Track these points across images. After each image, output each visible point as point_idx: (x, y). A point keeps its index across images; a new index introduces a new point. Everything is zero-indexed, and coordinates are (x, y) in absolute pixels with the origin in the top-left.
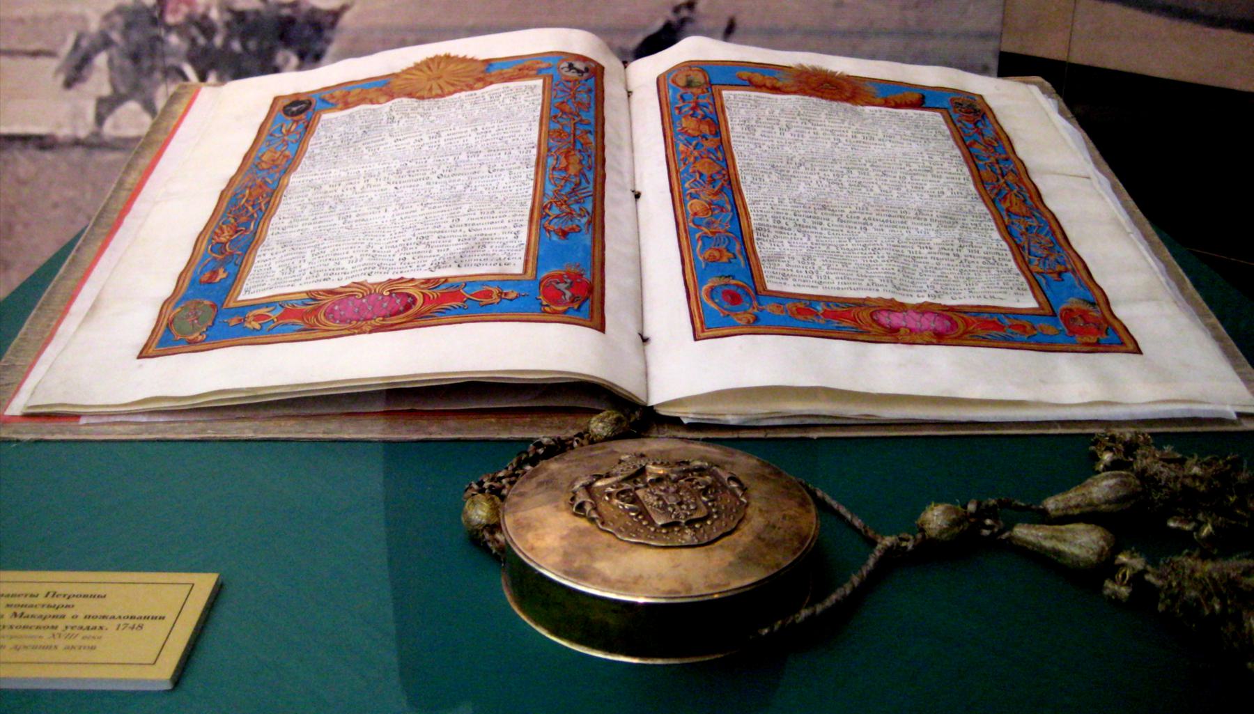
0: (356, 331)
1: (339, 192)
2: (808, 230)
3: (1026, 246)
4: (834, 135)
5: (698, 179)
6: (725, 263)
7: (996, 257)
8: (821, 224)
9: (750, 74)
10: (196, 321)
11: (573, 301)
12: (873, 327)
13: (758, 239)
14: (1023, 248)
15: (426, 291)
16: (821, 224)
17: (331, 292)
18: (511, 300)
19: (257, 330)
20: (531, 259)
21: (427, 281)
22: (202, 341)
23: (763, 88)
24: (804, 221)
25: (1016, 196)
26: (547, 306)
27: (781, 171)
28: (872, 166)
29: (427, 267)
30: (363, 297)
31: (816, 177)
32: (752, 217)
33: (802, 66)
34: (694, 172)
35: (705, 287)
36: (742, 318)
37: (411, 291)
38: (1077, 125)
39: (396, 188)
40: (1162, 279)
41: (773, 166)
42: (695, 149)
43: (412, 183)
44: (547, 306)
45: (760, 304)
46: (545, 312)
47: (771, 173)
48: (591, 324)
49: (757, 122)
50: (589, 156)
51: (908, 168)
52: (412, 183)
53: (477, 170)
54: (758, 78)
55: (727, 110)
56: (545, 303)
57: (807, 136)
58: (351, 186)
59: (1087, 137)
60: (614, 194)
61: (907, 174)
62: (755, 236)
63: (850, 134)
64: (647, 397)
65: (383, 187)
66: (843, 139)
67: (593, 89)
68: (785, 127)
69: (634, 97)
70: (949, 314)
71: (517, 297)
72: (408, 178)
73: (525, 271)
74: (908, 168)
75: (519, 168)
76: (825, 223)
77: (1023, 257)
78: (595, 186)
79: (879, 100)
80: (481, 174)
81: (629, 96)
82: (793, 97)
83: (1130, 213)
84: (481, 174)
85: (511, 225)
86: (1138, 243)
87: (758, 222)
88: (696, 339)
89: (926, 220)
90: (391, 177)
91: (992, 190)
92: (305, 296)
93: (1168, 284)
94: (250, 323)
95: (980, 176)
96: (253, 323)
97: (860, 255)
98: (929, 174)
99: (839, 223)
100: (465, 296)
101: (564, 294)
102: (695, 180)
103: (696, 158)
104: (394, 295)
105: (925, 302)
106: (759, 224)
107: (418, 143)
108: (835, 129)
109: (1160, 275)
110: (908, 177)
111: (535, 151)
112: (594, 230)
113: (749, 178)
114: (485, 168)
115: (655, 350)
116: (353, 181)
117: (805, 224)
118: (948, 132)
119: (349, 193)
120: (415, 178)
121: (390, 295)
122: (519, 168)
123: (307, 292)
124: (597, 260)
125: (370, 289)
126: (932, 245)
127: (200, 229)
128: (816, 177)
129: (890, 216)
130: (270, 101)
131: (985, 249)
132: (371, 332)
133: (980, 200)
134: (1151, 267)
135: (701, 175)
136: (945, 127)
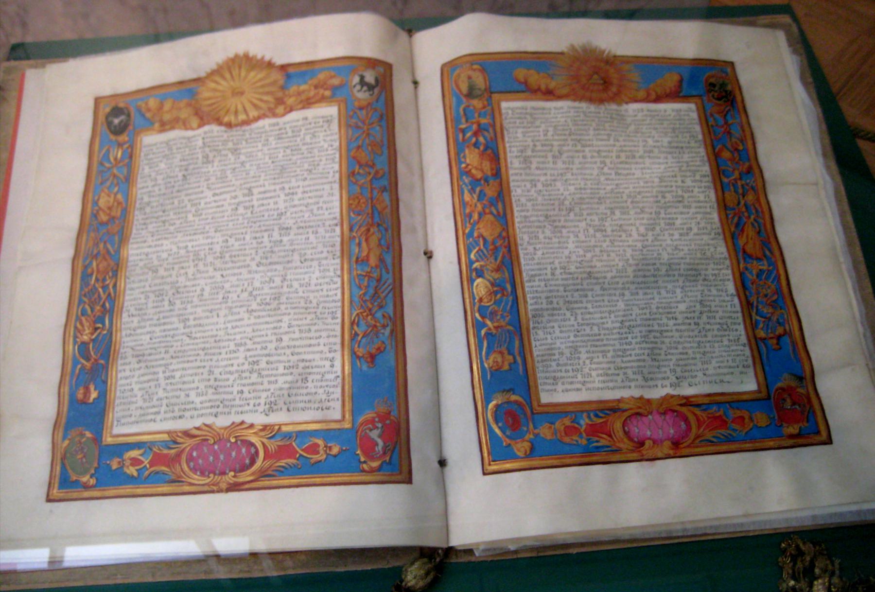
0: (215, 488)
1: (174, 278)
2: (576, 306)
3: (755, 304)
4: (600, 157)
5: (482, 247)
6: (506, 371)
7: (729, 321)
8: (586, 296)
9: (526, 71)
10: (84, 460)
11: (384, 453)
12: (624, 443)
13: (534, 328)
14: (752, 305)
15: (265, 441)
16: (586, 296)
17: (187, 434)
18: (335, 456)
19: (136, 478)
20: (347, 399)
21: (265, 428)
22: (93, 486)
23: (539, 93)
24: (572, 296)
25: (752, 224)
26: (365, 462)
27: (554, 221)
28: (632, 202)
29: (261, 409)
30: (215, 443)
31: (583, 225)
32: (530, 301)
33: (573, 47)
34: (478, 237)
35: (491, 406)
36: (521, 447)
37: (254, 440)
38: (815, 96)
39: (222, 276)
40: (861, 330)
41: (547, 217)
42: (478, 200)
43: (236, 271)
44: (365, 462)
45: (535, 427)
46: (363, 471)
47: (545, 226)
48: (399, 478)
49: (533, 151)
50: (386, 230)
51: (663, 201)
52: (236, 271)
53: (290, 259)
54: (535, 78)
55: (505, 133)
56: (363, 459)
57: (577, 161)
58: (183, 271)
59: (821, 115)
60: (411, 267)
61: (661, 208)
62: (531, 326)
63: (614, 154)
64: (446, 529)
65: (211, 274)
66: (608, 161)
67: (388, 188)
68: (557, 153)
69: (421, 87)
70: (684, 410)
71: (339, 453)
72: (230, 265)
73: (344, 416)
74: (663, 201)
75: (326, 258)
76: (590, 294)
77: (751, 316)
78: (394, 274)
79: (642, 94)
80: (294, 264)
81: (416, 88)
82: (564, 104)
83: (850, 244)
84: (294, 264)
85: (326, 349)
86: (846, 274)
87: (534, 307)
88: (484, 474)
89: (674, 276)
90: (216, 262)
91: (733, 218)
92: (165, 437)
93: (865, 336)
94: (128, 467)
95: (724, 200)
96: (131, 468)
97: (617, 336)
98: (680, 205)
99: (602, 292)
100: (297, 452)
101: (377, 444)
102: (480, 249)
103: (480, 214)
104: (239, 442)
105: (667, 394)
106: (537, 310)
107: (233, 201)
108: (601, 148)
109: (860, 326)
110: (662, 211)
111: (338, 230)
112: (396, 341)
113: (526, 237)
114: (296, 257)
115: (452, 470)
116: (184, 265)
117: (573, 299)
118: (700, 137)
119: (182, 279)
120: (238, 265)
121: (236, 441)
122: (326, 258)
123: (169, 433)
124: (401, 380)
125: (219, 434)
126: (678, 315)
127: (63, 320)
128: (583, 225)
129: (645, 276)
130: (91, 104)
131: (720, 314)
132: (228, 490)
133: (722, 237)
134: (854, 318)
135: (484, 239)
136: (698, 128)
